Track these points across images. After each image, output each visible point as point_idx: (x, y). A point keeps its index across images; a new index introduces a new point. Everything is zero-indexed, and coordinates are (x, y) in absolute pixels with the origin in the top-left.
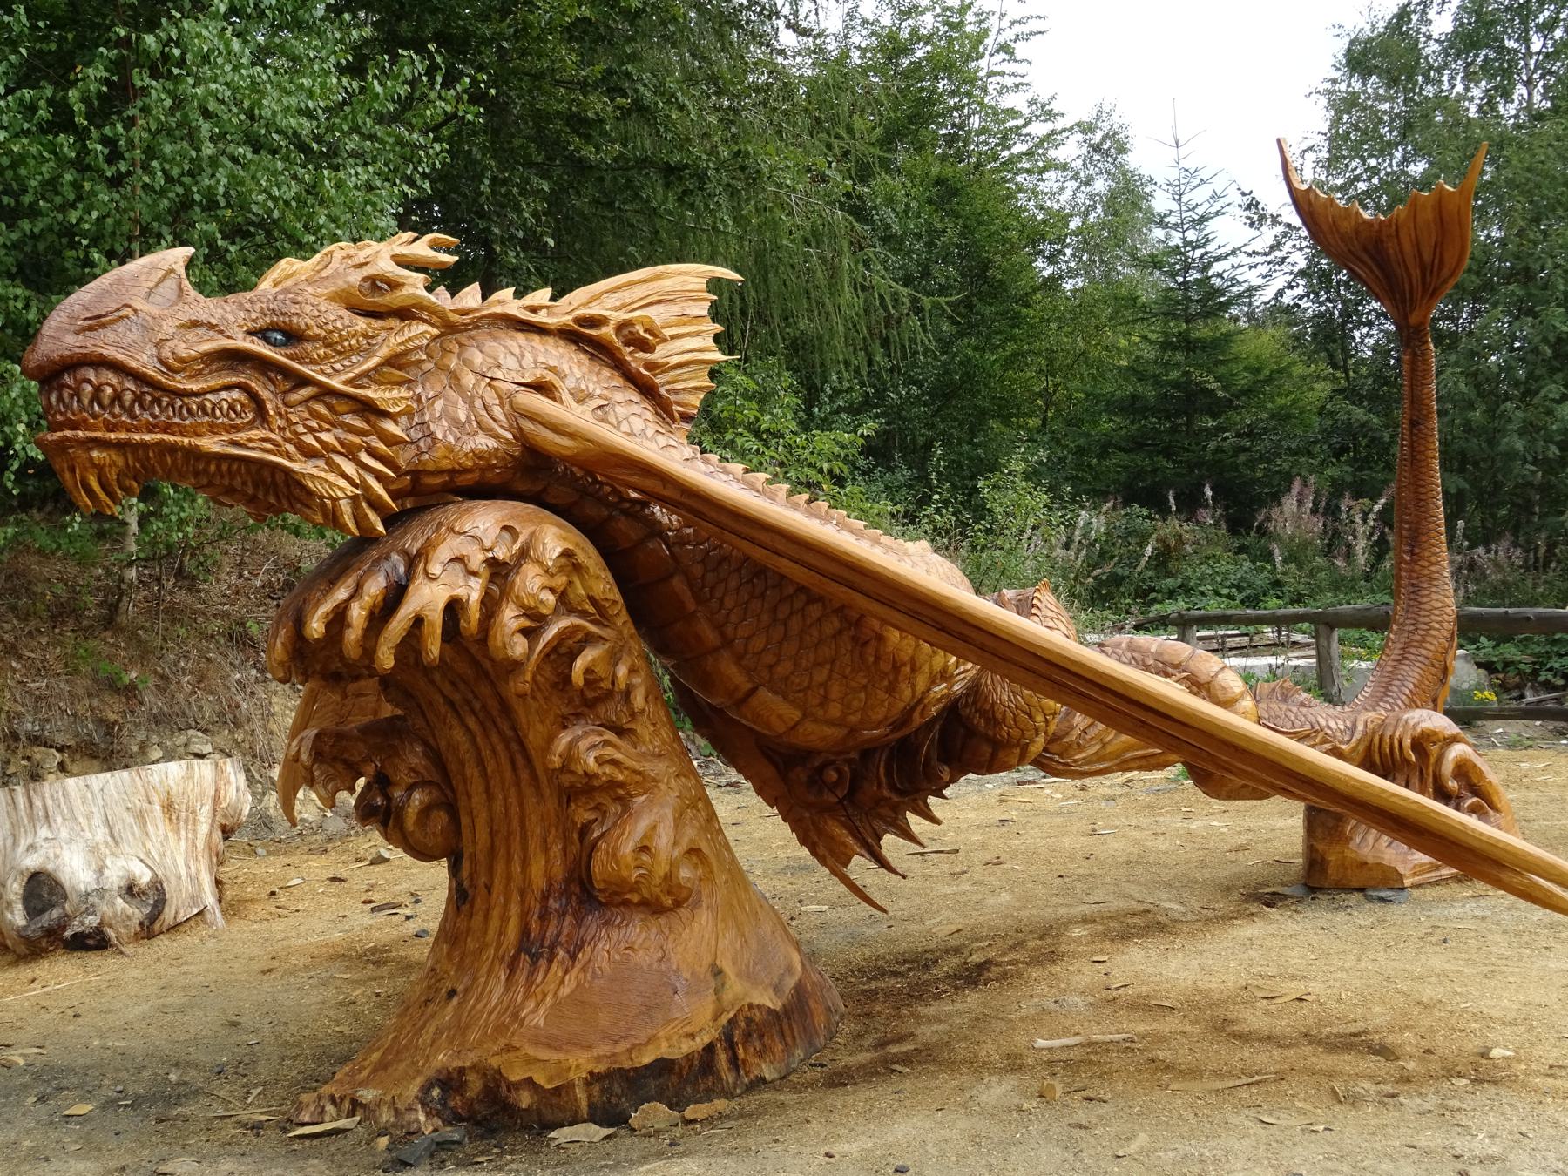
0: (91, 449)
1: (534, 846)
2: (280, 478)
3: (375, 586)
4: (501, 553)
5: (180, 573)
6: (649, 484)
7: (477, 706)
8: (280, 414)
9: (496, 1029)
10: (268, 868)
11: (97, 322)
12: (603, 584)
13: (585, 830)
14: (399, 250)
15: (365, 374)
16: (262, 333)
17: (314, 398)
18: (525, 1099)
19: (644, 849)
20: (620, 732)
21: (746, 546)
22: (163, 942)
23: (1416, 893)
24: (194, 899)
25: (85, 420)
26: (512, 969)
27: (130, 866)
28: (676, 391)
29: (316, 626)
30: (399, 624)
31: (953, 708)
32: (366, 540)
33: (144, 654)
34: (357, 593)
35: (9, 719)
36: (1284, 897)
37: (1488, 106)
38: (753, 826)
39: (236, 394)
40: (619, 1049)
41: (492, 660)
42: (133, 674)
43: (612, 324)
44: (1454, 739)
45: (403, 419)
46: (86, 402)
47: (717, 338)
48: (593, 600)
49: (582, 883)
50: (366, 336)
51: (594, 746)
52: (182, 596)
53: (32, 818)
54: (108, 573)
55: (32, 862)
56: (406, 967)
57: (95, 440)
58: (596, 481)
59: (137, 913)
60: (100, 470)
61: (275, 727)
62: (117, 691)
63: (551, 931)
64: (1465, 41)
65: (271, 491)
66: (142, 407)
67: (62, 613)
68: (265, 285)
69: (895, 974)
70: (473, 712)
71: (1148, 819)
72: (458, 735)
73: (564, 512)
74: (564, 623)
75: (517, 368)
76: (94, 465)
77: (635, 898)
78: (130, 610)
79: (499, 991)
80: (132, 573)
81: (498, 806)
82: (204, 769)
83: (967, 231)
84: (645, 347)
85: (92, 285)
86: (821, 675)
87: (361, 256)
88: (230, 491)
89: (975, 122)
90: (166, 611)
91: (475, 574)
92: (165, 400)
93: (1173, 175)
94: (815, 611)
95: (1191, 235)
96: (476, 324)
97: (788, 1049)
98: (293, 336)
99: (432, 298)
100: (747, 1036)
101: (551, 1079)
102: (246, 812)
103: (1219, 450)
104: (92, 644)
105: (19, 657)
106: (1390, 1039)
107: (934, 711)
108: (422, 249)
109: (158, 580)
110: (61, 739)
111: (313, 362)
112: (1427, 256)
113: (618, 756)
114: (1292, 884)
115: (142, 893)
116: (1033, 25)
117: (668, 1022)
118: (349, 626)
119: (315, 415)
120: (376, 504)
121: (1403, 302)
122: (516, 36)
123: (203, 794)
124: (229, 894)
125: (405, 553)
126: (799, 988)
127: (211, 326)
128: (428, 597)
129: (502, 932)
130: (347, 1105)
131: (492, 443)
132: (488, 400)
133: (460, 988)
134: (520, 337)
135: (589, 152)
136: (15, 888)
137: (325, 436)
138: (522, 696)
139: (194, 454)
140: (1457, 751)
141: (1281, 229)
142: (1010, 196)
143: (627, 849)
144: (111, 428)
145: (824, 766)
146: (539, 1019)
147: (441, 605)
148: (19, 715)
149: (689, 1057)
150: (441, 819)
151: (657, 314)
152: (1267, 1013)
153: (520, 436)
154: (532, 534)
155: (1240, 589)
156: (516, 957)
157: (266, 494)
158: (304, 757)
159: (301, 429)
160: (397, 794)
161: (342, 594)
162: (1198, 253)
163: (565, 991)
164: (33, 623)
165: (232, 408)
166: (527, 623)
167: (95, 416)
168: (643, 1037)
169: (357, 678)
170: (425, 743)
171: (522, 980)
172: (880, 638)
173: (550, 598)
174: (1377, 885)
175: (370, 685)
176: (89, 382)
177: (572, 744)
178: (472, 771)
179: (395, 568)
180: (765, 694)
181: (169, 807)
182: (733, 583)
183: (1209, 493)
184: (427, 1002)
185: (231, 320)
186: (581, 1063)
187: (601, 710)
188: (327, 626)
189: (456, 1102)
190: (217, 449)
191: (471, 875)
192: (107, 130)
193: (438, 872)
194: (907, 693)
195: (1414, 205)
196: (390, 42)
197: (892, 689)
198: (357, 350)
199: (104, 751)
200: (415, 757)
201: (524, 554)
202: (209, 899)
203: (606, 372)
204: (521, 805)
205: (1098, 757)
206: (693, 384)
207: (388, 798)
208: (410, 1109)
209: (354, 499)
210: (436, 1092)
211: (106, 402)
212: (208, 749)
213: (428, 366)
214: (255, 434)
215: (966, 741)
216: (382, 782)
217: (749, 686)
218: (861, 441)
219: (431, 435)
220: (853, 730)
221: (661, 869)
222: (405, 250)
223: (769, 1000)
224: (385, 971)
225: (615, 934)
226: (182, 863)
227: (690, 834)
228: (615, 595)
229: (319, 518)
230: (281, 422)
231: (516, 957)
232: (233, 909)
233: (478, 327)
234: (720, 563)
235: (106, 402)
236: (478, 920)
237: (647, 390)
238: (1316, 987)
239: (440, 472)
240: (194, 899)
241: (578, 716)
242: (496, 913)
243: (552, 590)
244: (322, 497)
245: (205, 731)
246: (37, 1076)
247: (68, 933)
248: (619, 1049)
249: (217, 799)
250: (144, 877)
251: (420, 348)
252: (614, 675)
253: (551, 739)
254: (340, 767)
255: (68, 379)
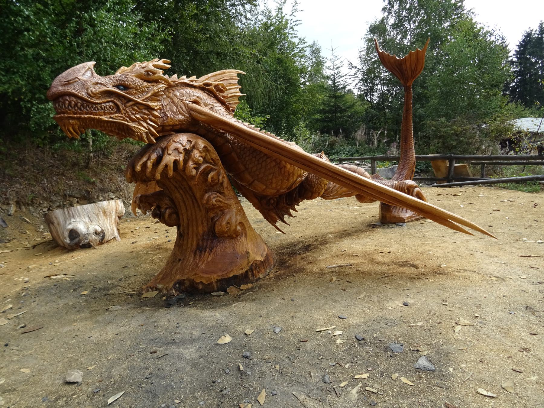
0: (69, 120)
1: (199, 223)
2: (125, 127)
3: (154, 157)
4: (188, 147)
5: (104, 154)
6: (226, 128)
7: (183, 187)
8: (124, 109)
9: (192, 269)
10: (132, 225)
11: (68, 83)
12: (215, 155)
13: (212, 219)
14: (154, 63)
15: (147, 98)
16: (117, 86)
17: (134, 105)
18: (201, 287)
19: (228, 223)
20: (220, 193)
21: (252, 144)
22: (105, 245)
23: (408, 223)
24: (112, 234)
25: (67, 111)
26: (195, 254)
27: (95, 227)
28: (230, 104)
29: (138, 168)
30: (161, 167)
31: (302, 184)
32: (150, 145)
33: (96, 174)
34: (149, 158)
35: (63, 191)
36: (376, 225)
37: (402, 40)
38: (252, 213)
39: (111, 104)
40: (224, 273)
41: (186, 176)
42: (94, 179)
43: (213, 85)
44: (416, 187)
45: (159, 111)
46: (67, 106)
47: (240, 89)
48: (212, 159)
49: (212, 232)
50: (147, 87)
51: (214, 197)
52: (105, 160)
53: (69, 216)
54: (86, 155)
55: (70, 227)
56: (166, 250)
57: (70, 117)
58: (211, 128)
59: (98, 238)
60: (73, 126)
61: (130, 191)
62: (90, 183)
63: (205, 244)
64: (395, 26)
65: (124, 131)
66: (84, 108)
67: (75, 165)
68: (118, 74)
69: (287, 248)
70: (182, 189)
71: (351, 210)
72: (178, 195)
73: (203, 136)
74: (205, 165)
75: (191, 95)
76: (71, 124)
77: (226, 235)
78: (92, 164)
79: (192, 259)
80: (92, 155)
81: (189, 213)
82: (112, 203)
83: (285, 70)
84: (222, 91)
85: (66, 72)
86: (270, 177)
87: (144, 65)
88: (111, 131)
89: (286, 45)
90: (101, 164)
91: (181, 153)
92: (90, 106)
93: (331, 57)
94: (269, 160)
95: (336, 71)
96: (177, 85)
97: (265, 270)
98: (126, 87)
99: (165, 77)
100: (256, 268)
101: (207, 282)
102: (124, 212)
103: (343, 121)
104: (83, 172)
105: (65, 176)
106: (415, 263)
107: (297, 185)
108: (161, 63)
109: (98, 156)
110: (77, 195)
111: (132, 95)
112: (413, 68)
113: (221, 200)
114: (377, 222)
115: (99, 234)
116: (298, 22)
117: (236, 266)
118: (148, 168)
119: (134, 110)
120: (153, 134)
121: (406, 80)
122: (180, 18)
123: (113, 209)
124: (121, 232)
125: (161, 148)
126: (267, 255)
127: (102, 84)
128: (169, 159)
129: (192, 245)
130: (154, 289)
131: (183, 117)
132: (182, 106)
133: (182, 259)
134: (189, 89)
135: (199, 49)
136: (66, 234)
137: (138, 116)
138: (195, 185)
139: (100, 121)
140: (417, 189)
141: (357, 69)
142: (294, 62)
143: (224, 223)
144: (75, 113)
145: (270, 199)
146: (203, 267)
147: (172, 162)
148: (65, 190)
149: (242, 274)
150: (174, 216)
151: (225, 83)
152: (382, 256)
153: (191, 115)
154: (196, 142)
155: (349, 152)
156: (196, 251)
157: (122, 132)
158: (137, 202)
159: (130, 114)
160: (163, 210)
161: (145, 159)
162: (338, 75)
163: (210, 259)
164: (68, 167)
165: (110, 107)
166: (196, 166)
167: (70, 110)
168: (230, 270)
169: (150, 181)
170: (169, 197)
171: (198, 257)
172: (285, 167)
173: (201, 159)
174: (398, 222)
175: (154, 183)
176: (67, 100)
177: (209, 197)
178: (182, 204)
179: (159, 152)
180: (256, 182)
181: (104, 212)
182: (248, 154)
183: (341, 131)
184: (173, 262)
185: (108, 83)
186: (214, 277)
187: (215, 188)
188: (141, 168)
189: (183, 287)
190: (106, 119)
191: (183, 230)
192: (77, 39)
193: (175, 228)
194: (292, 181)
195: (411, 54)
196: (147, 19)
197: (288, 180)
198: (144, 91)
199: (88, 198)
200: (167, 201)
201: (194, 147)
202: (116, 234)
203: (212, 98)
204: (195, 213)
205: (336, 194)
206: (234, 102)
207: (160, 212)
208: (171, 290)
209: (146, 133)
210: (177, 286)
211: (73, 106)
212: (114, 197)
213: (165, 96)
214: (117, 115)
215: (306, 191)
216: (158, 207)
217: (252, 180)
218: (266, 119)
219: (166, 115)
220: (278, 191)
221: (233, 228)
222: (156, 63)
223: (260, 258)
224: (161, 251)
225: (221, 245)
226: (109, 226)
227: (239, 218)
228: (218, 158)
229: (137, 138)
230: (125, 112)
231: (196, 251)
232: (122, 236)
233: (177, 86)
234: (244, 149)
235: (73, 106)
236: (185, 242)
237: (223, 103)
238: (392, 250)
239: (169, 126)
240: (112, 234)
241: (209, 189)
242: (190, 240)
243: (202, 157)
244: (137, 133)
245: (113, 192)
246: (73, 284)
247: (81, 244)
248: (224, 273)
249: (116, 210)
250: (99, 230)
251: (162, 91)
252: (219, 178)
253: (203, 196)
254: (147, 204)
255: (61, 100)
